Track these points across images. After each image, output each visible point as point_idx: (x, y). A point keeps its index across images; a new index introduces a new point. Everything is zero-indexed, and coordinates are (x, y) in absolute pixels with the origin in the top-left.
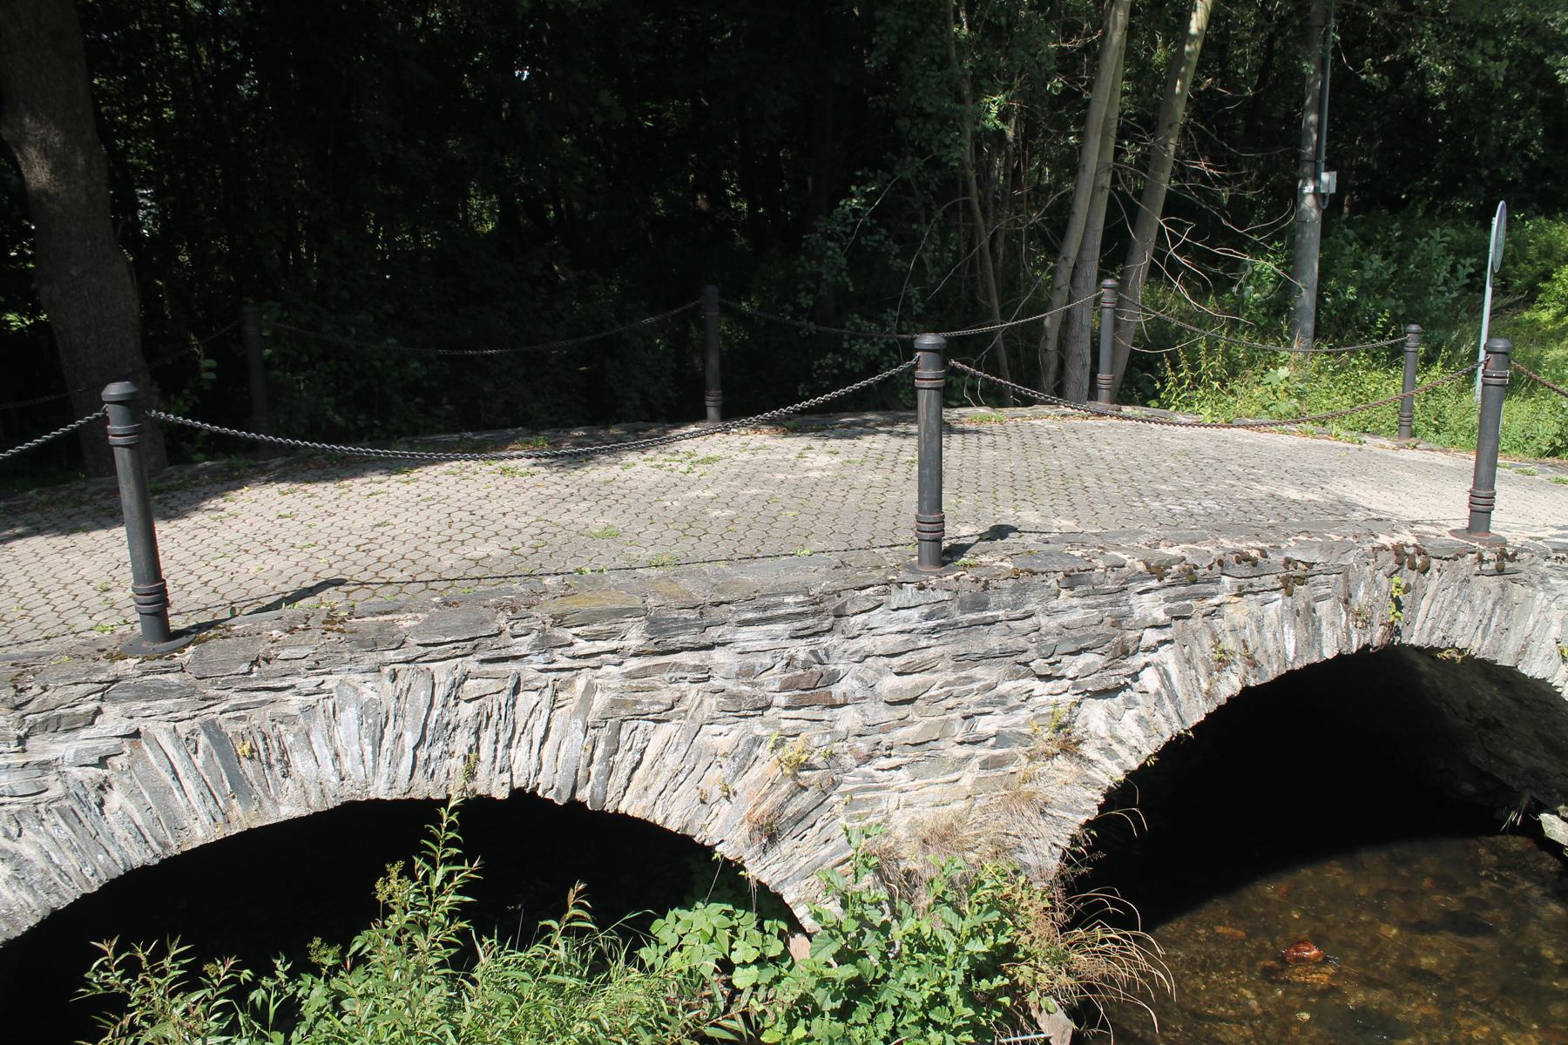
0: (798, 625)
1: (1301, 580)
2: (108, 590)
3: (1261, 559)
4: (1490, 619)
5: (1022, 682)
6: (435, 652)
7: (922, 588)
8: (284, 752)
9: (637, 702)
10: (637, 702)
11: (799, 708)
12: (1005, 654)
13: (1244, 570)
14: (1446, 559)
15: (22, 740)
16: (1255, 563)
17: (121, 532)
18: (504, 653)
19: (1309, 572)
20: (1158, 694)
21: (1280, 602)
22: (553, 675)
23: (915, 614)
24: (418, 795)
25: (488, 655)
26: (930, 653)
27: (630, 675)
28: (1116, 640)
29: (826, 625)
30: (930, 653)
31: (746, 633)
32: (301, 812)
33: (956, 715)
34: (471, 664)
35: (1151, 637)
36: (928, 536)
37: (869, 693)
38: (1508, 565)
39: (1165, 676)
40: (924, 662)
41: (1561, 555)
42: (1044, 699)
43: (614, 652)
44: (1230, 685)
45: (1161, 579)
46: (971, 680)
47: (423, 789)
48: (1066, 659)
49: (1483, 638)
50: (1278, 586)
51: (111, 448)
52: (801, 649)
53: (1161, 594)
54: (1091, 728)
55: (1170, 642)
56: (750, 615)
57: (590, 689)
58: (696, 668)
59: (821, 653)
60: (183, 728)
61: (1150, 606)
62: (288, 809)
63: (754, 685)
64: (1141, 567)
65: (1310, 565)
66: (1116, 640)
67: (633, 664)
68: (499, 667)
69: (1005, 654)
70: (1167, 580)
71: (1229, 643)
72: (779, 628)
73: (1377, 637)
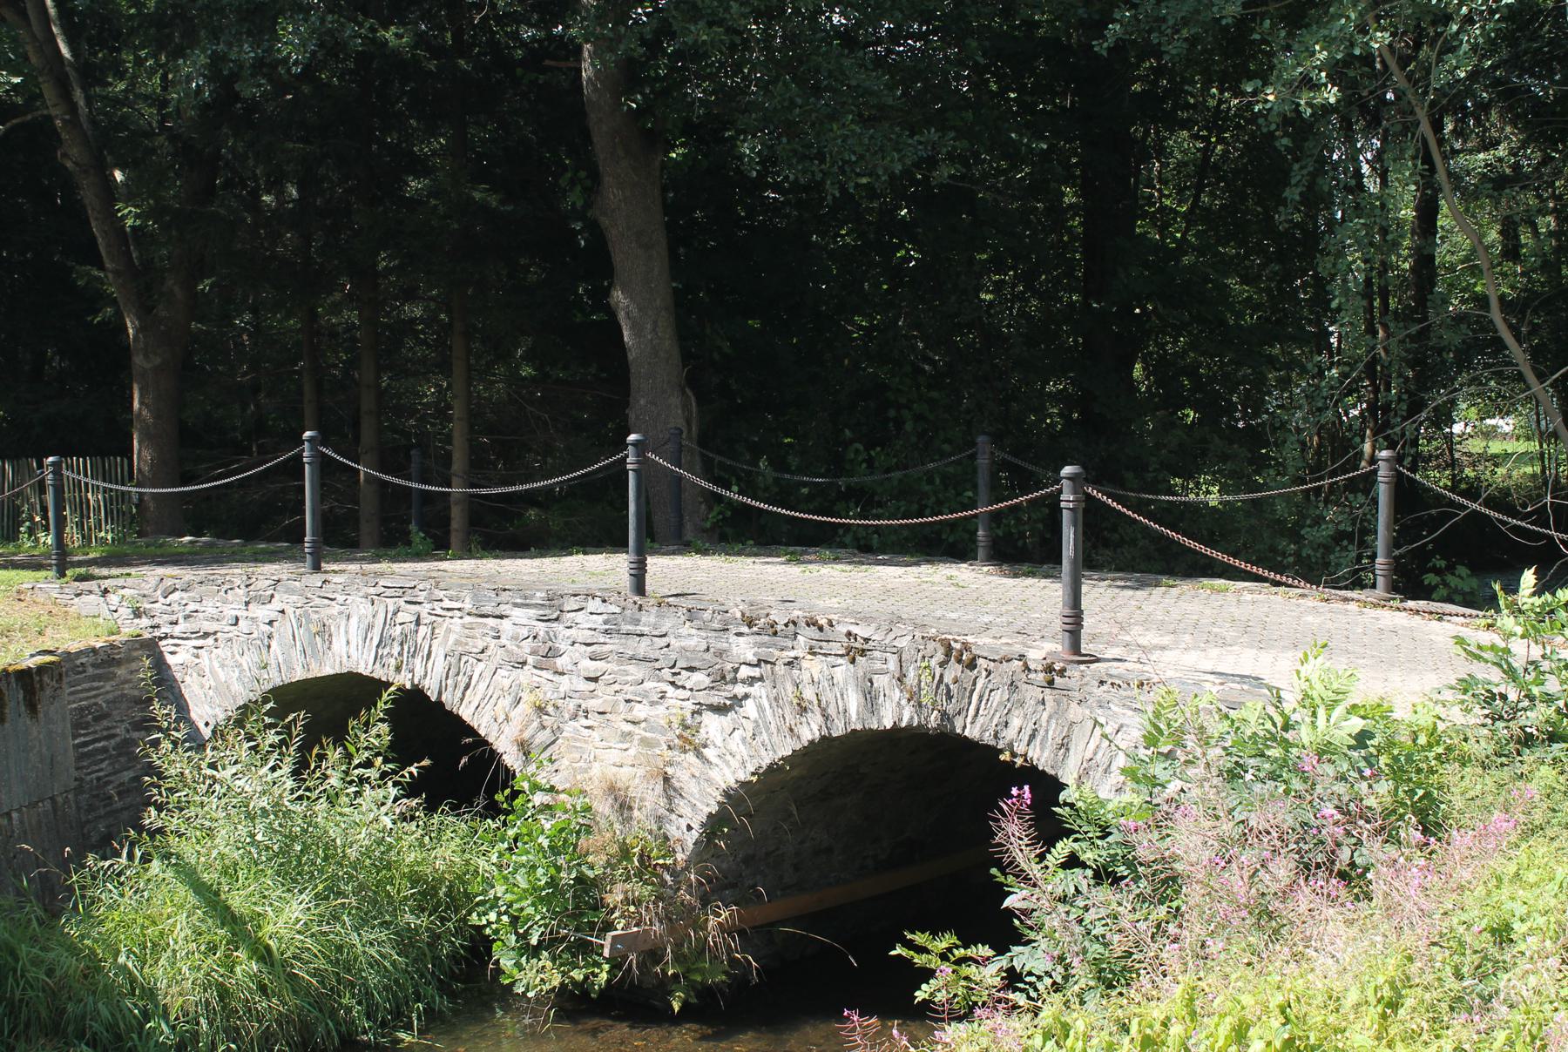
0: (541, 612)
1: (863, 652)
2: (1440, 718)
3: (826, 627)
4: (1047, 731)
5: (660, 684)
6: (389, 592)
7: (604, 601)
8: (330, 635)
9: (467, 644)
10: (467, 644)
11: (542, 669)
12: (645, 660)
13: (813, 632)
14: (994, 661)
15: (247, 603)
16: (821, 629)
17: (1058, 586)
18: (414, 599)
19: (865, 647)
20: (756, 721)
21: (844, 667)
22: (434, 618)
23: (600, 619)
24: (375, 675)
25: (409, 599)
26: (606, 648)
27: (464, 626)
28: (717, 667)
29: (554, 616)
30: (606, 648)
31: (517, 612)
32: (332, 672)
33: (620, 697)
34: (401, 602)
35: (745, 672)
36: (1067, 627)
37: (574, 668)
38: (1058, 680)
39: (760, 708)
40: (602, 653)
41: (1117, 682)
42: (674, 701)
43: (459, 609)
44: (810, 731)
45: (750, 627)
46: (626, 673)
47: (380, 674)
48: (683, 672)
49: (1042, 750)
50: (840, 652)
51: (627, 471)
52: (541, 628)
53: (751, 639)
54: (711, 736)
55: (761, 679)
56: (519, 601)
57: (449, 631)
58: (492, 629)
59: (551, 634)
60: (298, 611)
61: (744, 648)
62: (328, 670)
63: (518, 647)
64: (739, 615)
65: (867, 640)
66: (717, 667)
67: (468, 619)
68: (413, 607)
69: (645, 660)
70: (755, 629)
71: (809, 694)
72: (532, 612)
73: (933, 721)
